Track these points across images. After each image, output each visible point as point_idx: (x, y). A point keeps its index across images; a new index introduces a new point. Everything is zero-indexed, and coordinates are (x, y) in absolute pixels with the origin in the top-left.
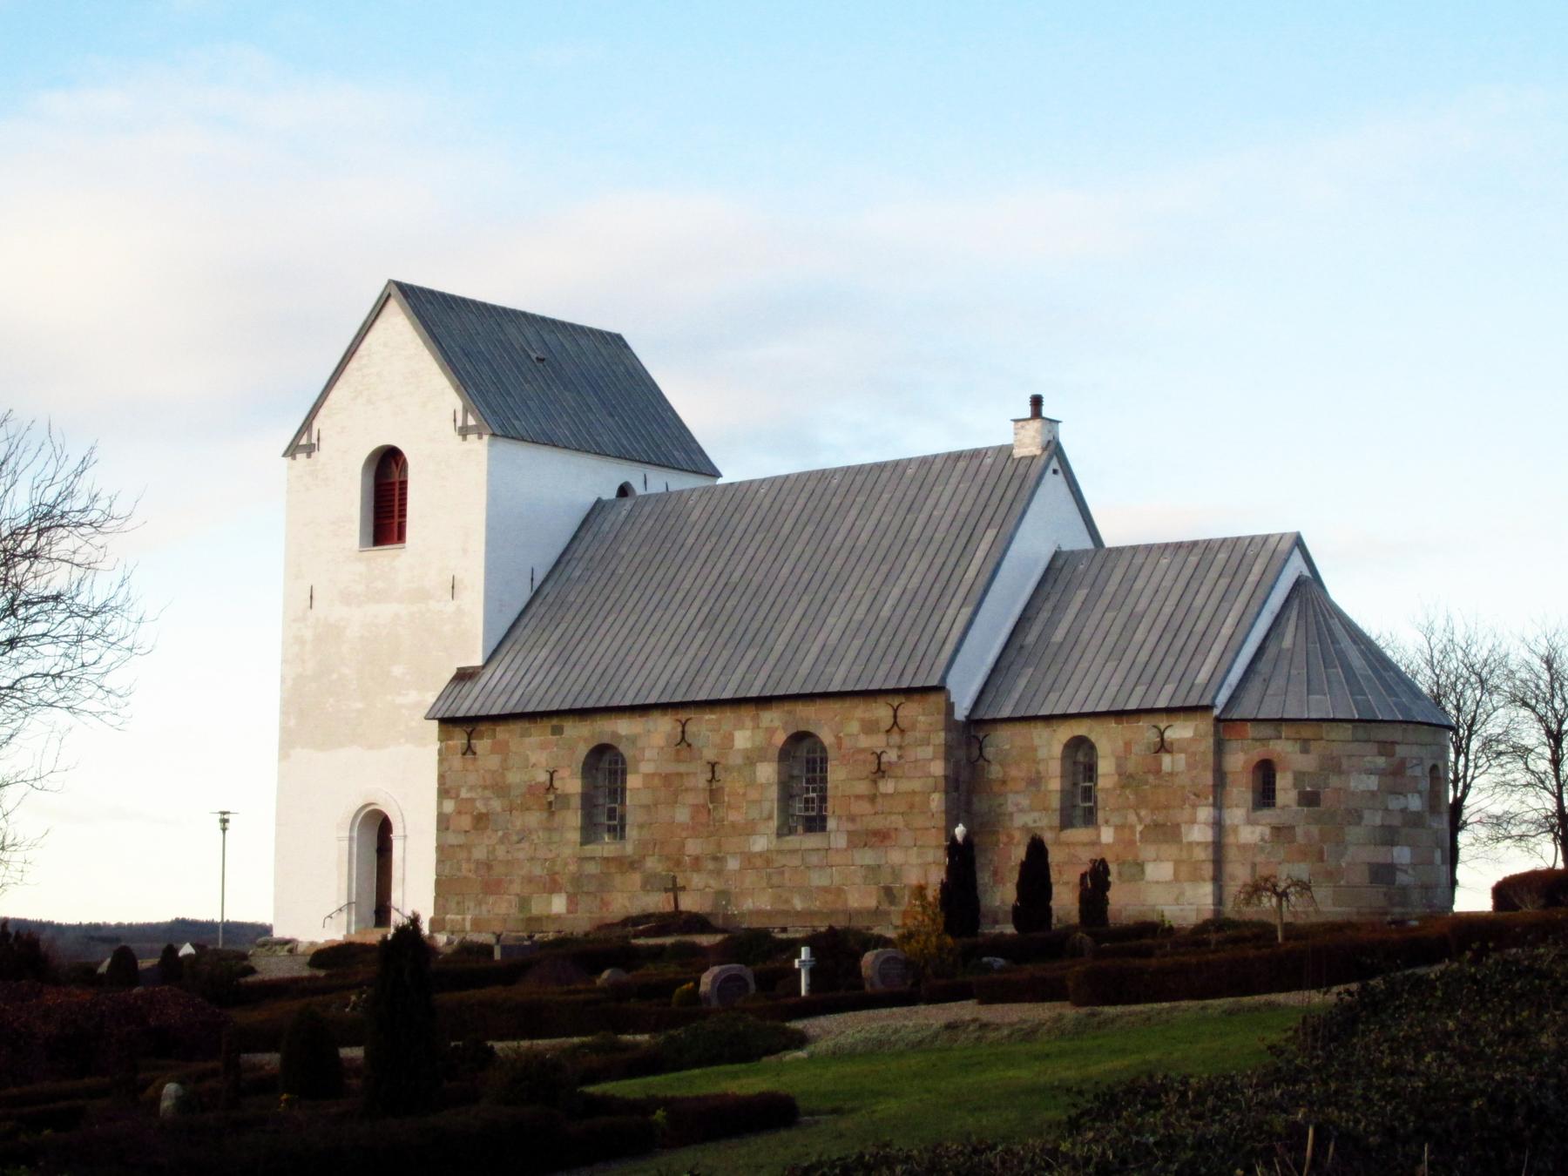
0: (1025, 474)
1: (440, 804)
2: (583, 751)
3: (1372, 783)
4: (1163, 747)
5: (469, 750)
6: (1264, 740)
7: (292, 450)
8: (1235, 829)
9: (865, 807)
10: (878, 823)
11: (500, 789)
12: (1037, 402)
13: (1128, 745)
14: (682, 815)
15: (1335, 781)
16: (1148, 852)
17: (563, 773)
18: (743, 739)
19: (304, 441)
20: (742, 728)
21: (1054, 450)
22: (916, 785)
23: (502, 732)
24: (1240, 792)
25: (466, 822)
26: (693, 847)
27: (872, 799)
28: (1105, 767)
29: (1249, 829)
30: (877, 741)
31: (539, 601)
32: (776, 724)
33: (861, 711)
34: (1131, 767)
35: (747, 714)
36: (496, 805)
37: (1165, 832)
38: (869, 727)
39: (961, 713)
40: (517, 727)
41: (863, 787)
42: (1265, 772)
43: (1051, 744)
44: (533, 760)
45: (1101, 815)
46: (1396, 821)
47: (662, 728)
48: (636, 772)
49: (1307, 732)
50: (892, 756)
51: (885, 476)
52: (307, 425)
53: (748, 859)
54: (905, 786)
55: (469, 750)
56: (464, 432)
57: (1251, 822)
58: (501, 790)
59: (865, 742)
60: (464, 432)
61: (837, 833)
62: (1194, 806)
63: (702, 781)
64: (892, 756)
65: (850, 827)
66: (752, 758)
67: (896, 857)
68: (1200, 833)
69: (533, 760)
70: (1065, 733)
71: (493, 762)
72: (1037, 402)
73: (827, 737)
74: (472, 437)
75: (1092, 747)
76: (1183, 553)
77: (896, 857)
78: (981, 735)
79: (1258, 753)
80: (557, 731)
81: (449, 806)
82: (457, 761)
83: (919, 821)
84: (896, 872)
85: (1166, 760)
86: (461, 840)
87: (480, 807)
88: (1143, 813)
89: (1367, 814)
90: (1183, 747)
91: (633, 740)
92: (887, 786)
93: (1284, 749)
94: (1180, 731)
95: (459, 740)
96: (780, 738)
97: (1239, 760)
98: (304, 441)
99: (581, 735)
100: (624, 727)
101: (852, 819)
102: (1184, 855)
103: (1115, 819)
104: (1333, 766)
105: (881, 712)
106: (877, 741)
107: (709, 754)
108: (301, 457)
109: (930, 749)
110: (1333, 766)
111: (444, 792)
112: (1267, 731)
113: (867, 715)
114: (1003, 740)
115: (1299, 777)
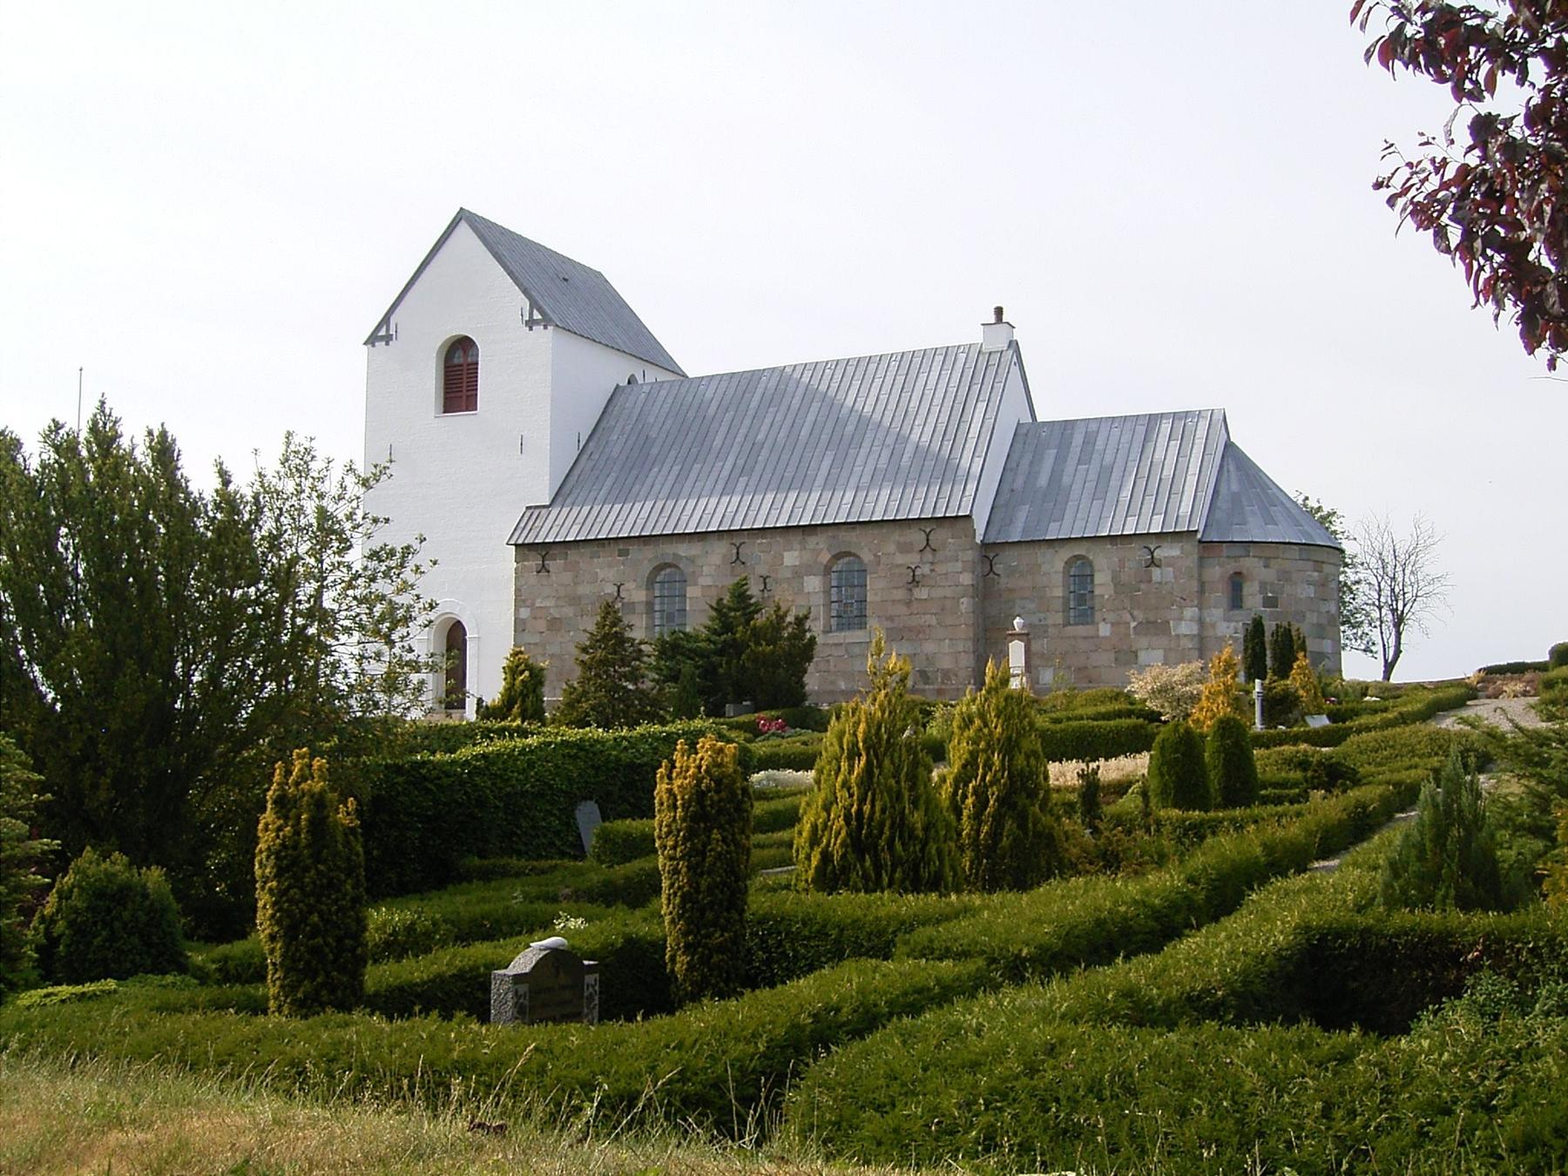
0: (999, 361)
1: (516, 610)
2: (646, 568)
3: (1311, 591)
4: (1153, 562)
5: (543, 568)
6: (1237, 558)
7: (372, 340)
8: (1213, 626)
9: (902, 610)
10: (914, 621)
11: (575, 600)
12: (999, 311)
13: (1122, 561)
15: (1287, 589)
16: (1143, 642)
17: (630, 585)
18: (791, 558)
19: (383, 332)
20: (791, 549)
21: (1014, 345)
22: (948, 592)
23: (573, 555)
24: (1219, 595)
25: (542, 625)
27: (909, 603)
28: (1102, 579)
29: (1225, 624)
30: (912, 559)
31: (585, 457)
32: (821, 549)
33: (897, 536)
34: (1124, 578)
35: (796, 539)
36: (569, 611)
37: (1156, 627)
38: (904, 548)
39: (979, 539)
40: (586, 551)
41: (900, 594)
42: (1236, 583)
43: (1055, 563)
44: (601, 576)
45: (1098, 616)
46: (1324, 621)
48: (696, 584)
49: (1268, 552)
50: (926, 569)
51: (872, 366)
52: (386, 320)
54: (938, 593)
55: (543, 568)
56: (530, 324)
57: (1228, 620)
58: (575, 600)
59: (900, 559)
60: (530, 324)
61: (876, 629)
62: (1181, 607)
65: (889, 624)
66: (798, 573)
67: (929, 647)
68: (1187, 628)
69: (601, 576)
70: (1066, 553)
71: (567, 577)
72: (999, 311)
73: (867, 556)
74: (538, 329)
75: (1091, 564)
76: (1128, 425)
77: (929, 647)
78: (991, 555)
79: (1231, 567)
81: (525, 613)
82: (532, 578)
83: (949, 620)
84: (929, 659)
85: (1156, 573)
86: (536, 639)
87: (555, 613)
88: (1136, 613)
89: (1308, 615)
90: (1171, 562)
91: (692, 560)
92: (922, 593)
93: (1250, 564)
94: (1166, 552)
95: (534, 562)
96: (825, 557)
97: (1217, 572)
98: (383, 332)
99: (646, 558)
100: (683, 550)
101: (891, 618)
102: (1173, 645)
103: (1111, 617)
104: (1285, 576)
105: (917, 537)
106: (912, 559)
107: (762, 570)
108: (380, 345)
109: (960, 564)
110: (1285, 576)
111: (520, 602)
112: (1238, 551)
113: (902, 539)
114: (1006, 562)
115: (1263, 586)
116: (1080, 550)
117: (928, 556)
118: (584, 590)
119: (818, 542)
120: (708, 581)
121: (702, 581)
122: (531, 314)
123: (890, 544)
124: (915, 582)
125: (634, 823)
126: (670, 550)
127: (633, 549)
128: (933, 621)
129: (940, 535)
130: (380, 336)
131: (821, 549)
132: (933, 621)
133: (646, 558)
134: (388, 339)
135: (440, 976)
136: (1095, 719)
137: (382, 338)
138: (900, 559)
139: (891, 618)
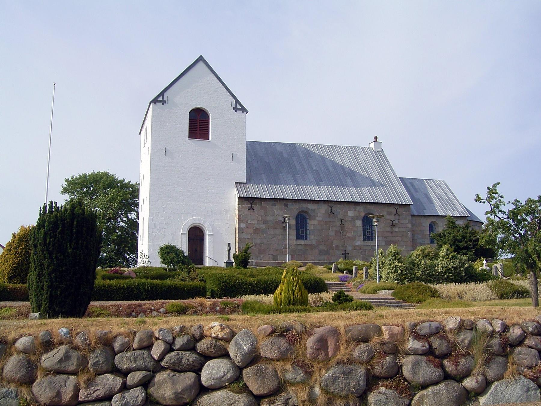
2: (296, 212)
7: (155, 101)
11: (266, 222)
14: (332, 233)
18: (351, 213)
22: (404, 230)
23: (264, 204)
25: (251, 231)
26: (336, 243)
27: (392, 232)
30: (392, 217)
33: (387, 209)
36: (263, 226)
38: (390, 214)
40: (271, 203)
41: (388, 229)
47: (324, 209)
50: (396, 221)
52: (162, 94)
53: (355, 247)
56: (236, 109)
58: (266, 222)
63: (338, 223)
64: (396, 221)
66: (354, 219)
80: (285, 205)
82: (246, 212)
91: (313, 210)
92: (396, 229)
95: (247, 205)
96: (363, 214)
98: (161, 99)
100: (310, 206)
105: (393, 210)
106: (392, 217)
111: (240, 220)
113: (388, 210)
116: (434, 220)
117: (397, 217)
118: (270, 218)
119: (360, 208)
120: (320, 219)
121: (318, 219)
122: (236, 105)
123: (384, 212)
124: (393, 225)
125: (193, 300)
126: (305, 206)
127: (290, 204)
128: (400, 239)
129: (401, 210)
130: (159, 100)
131: (362, 212)
132: (400, 239)
133: (295, 209)
134: (163, 102)
135: (79, 318)
136: (110, 278)
137: (160, 101)
138: (388, 217)
139: (386, 237)
